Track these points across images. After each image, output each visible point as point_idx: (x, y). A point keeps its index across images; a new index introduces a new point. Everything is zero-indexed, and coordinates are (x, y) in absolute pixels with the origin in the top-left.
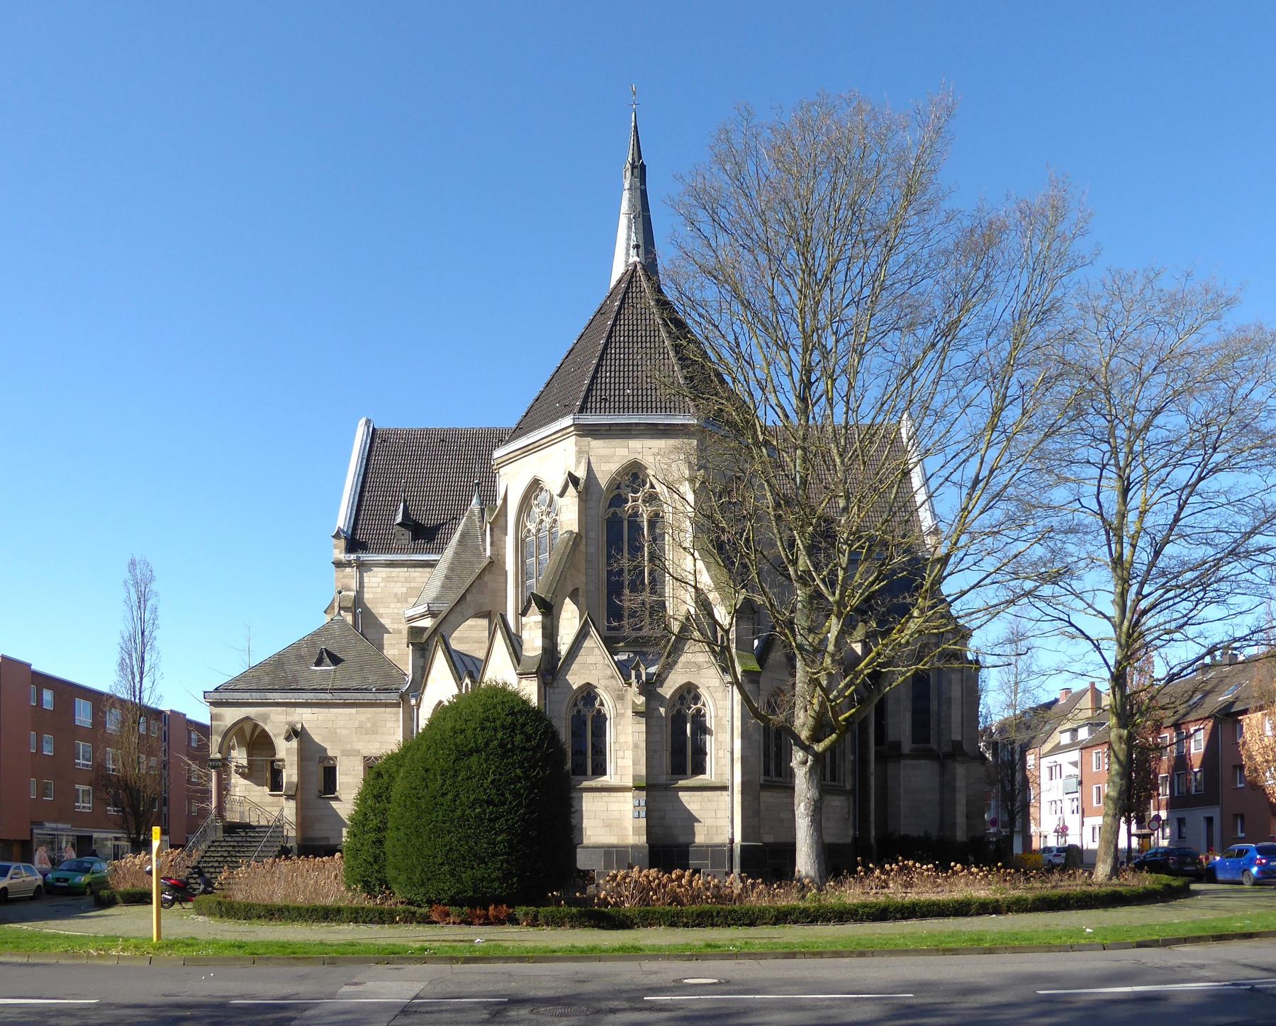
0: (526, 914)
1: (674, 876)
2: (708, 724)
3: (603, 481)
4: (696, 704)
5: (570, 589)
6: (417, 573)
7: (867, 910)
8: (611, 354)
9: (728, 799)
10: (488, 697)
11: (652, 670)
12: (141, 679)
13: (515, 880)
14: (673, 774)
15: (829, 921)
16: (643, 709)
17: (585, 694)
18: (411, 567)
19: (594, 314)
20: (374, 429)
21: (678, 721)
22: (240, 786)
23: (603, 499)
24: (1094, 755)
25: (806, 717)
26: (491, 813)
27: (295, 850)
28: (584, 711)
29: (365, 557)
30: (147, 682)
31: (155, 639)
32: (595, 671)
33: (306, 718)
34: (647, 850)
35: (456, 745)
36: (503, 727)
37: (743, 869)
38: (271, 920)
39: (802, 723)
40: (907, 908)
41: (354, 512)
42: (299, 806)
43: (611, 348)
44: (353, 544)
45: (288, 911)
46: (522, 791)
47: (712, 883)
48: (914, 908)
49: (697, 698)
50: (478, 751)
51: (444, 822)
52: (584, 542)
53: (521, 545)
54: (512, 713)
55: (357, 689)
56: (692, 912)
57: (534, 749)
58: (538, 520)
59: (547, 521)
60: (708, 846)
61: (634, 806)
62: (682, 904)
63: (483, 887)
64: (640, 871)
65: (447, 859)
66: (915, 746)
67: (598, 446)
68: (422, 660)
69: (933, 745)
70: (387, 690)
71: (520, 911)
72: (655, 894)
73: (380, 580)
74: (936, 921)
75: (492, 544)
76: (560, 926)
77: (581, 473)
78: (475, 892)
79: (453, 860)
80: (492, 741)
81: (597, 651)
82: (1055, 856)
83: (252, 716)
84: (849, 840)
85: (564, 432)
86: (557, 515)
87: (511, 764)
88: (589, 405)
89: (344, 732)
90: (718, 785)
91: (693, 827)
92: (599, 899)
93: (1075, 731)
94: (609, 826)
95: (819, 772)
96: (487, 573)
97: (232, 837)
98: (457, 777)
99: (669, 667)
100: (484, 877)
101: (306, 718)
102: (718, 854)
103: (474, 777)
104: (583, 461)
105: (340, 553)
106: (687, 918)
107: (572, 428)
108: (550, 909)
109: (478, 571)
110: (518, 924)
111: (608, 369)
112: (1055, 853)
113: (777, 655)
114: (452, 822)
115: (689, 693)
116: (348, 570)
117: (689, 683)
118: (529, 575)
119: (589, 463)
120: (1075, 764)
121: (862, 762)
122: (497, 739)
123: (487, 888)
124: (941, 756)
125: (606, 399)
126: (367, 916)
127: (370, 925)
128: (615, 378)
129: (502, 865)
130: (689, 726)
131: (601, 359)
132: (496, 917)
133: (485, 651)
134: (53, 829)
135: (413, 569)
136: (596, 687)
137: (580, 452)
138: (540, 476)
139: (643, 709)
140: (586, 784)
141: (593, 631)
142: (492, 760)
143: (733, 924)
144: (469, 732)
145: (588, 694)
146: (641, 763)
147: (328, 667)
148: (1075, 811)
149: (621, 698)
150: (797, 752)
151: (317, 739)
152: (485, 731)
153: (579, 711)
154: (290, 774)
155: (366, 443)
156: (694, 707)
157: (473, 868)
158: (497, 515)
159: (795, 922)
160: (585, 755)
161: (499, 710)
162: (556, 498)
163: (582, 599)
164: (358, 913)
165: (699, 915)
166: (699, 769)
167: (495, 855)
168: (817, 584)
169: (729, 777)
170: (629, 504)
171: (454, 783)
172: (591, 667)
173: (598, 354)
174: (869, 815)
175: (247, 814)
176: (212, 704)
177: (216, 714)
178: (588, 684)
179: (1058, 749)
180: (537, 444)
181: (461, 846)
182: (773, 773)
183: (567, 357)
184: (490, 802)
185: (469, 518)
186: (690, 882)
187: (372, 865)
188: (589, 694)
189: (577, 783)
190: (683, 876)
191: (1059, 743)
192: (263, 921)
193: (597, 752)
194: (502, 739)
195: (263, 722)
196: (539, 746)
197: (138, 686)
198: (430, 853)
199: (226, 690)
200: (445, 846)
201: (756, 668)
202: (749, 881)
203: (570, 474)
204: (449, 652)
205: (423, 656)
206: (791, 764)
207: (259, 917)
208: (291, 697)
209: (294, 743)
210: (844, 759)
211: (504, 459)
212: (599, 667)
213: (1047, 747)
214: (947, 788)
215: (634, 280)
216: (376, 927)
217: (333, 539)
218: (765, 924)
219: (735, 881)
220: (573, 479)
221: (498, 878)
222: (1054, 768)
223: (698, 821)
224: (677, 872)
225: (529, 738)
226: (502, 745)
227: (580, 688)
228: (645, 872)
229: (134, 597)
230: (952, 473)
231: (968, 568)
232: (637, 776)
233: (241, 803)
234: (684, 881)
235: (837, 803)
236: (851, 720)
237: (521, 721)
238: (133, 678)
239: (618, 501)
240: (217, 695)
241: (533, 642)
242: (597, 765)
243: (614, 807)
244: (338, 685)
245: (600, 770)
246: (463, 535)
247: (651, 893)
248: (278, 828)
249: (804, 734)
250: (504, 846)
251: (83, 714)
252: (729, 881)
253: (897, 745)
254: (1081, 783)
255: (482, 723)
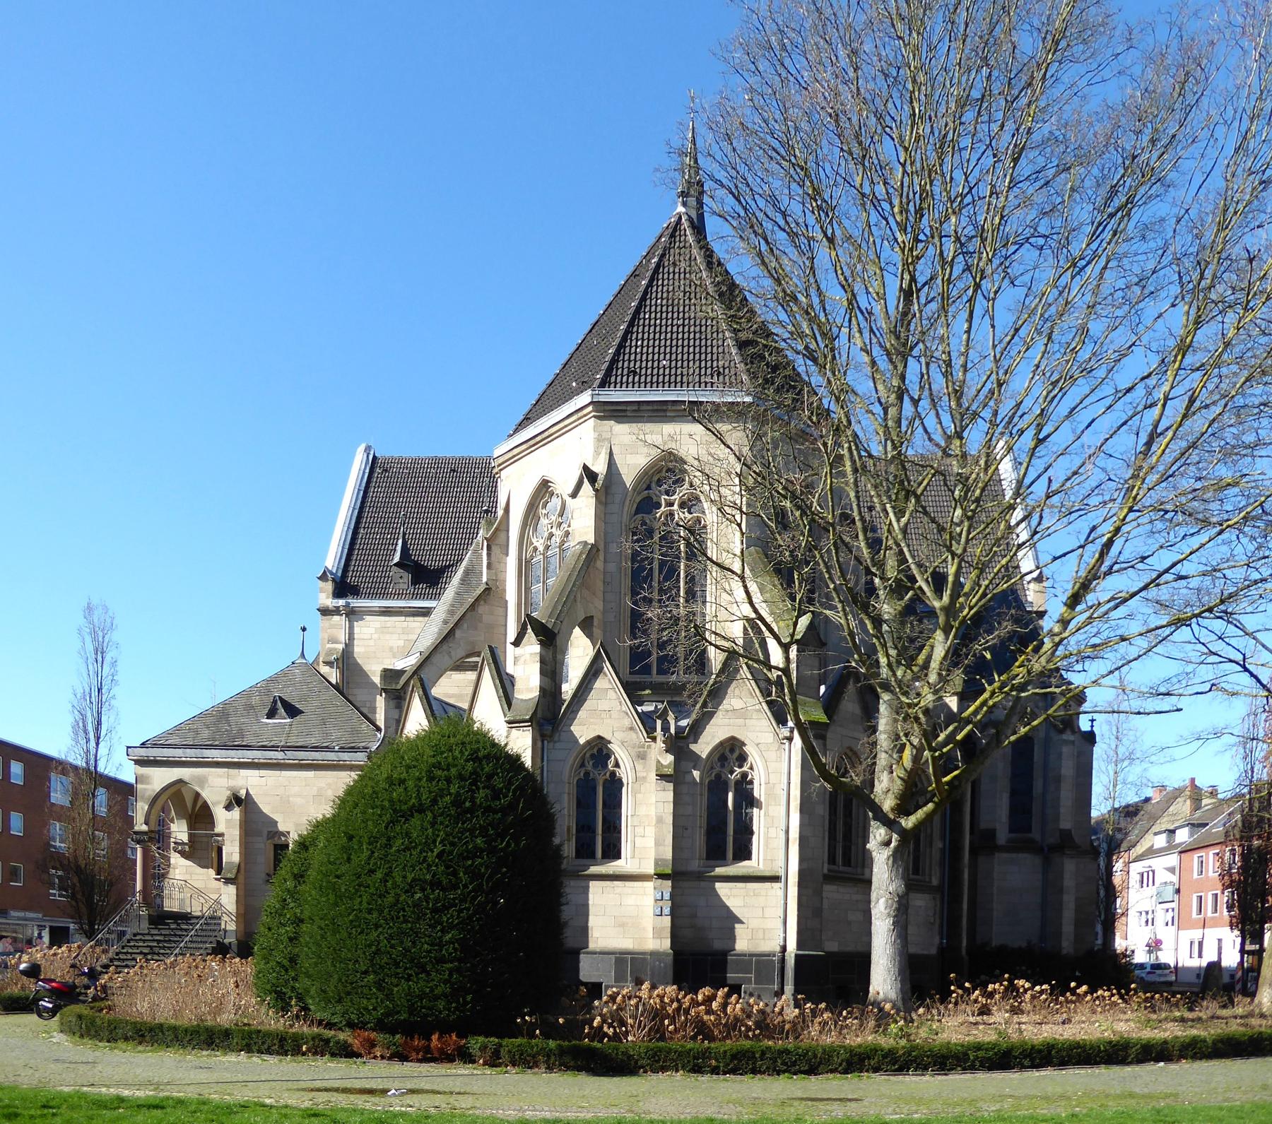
0: (483, 1048)
1: (700, 997)
2: (756, 794)
3: (629, 476)
4: (741, 767)
5: (581, 616)
6: (416, 623)
7: (981, 1054)
8: (645, 319)
9: (781, 893)
10: (443, 736)
11: (684, 723)
12: (97, 744)
13: (469, 998)
14: (708, 858)
15: (925, 1068)
16: (670, 771)
17: (595, 750)
18: (409, 616)
19: (626, 278)
20: (375, 458)
21: (717, 787)
22: (181, 868)
23: (627, 503)
24: (1196, 860)
25: (892, 780)
26: (437, 900)
27: (235, 948)
28: (594, 773)
29: (356, 603)
30: (103, 750)
31: (114, 697)
32: (609, 721)
33: (250, 782)
34: (671, 958)
35: (391, 801)
36: (461, 777)
37: (797, 991)
38: (140, 1043)
39: (886, 790)
40: (1040, 1051)
41: (346, 551)
42: (242, 893)
43: (645, 313)
44: (343, 588)
45: (162, 1032)
46: (483, 870)
47: (756, 1007)
48: (1049, 1052)
49: (742, 758)
50: (421, 810)
51: (370, 912)
52: (601, 557)
53: (525, 567)
54: (474, 757)
55: (316, 747)
56: (725, 1052)
57: (504, 811)
58: (546, 535)
59: (558, 533)
60: (752, 955)
61: (656, 900)
62: (712, 1039)
63: (422, 1007)
64: (653, 987)
65: (373, 965)
66: (1013, 835)
67: (622, 432)
68: (397, 711)
69: (1036, 835)
70: (354, 749)
71: (475, 1043)
72: (673, 1022)
73: (373, 631)
74: (1083, 1071)
75: (489, 566)
76: (530, 1068)
77: (600, 468)
78: (411, 1013)
79: (381, 967)
80: (442, 797)
81: (611, 694)
82: (1149, 973)
83: (186, 779)
84: (933, 951)
85: (580, 414)
86: (569, 526)
87: (469, 830)
88: (613, 379)
89: (299, 800)
90: (767, 874)
91: (733, 929)
92: (591, 1027)
93: (1172, 832)
94: (622, 925)
95: (905, 857)
96: (482, 602)
97: (159, 929)
98: (391, 847)
99: (706, 717)
100: (424, 993)
101: (250, 782)
102: (765, 965)
103: (415, 848)
104: (604, 450)
105: (328, 598)
106: (717, 1060)
107: (590, 408)
108: (519, 1041)
109: (471, 600)
110: (473, 1062)
111: (640, 336)
112: (1148, 969)
113: (850, 705)
114: (381, 912)
115: (732, 751)
116: (336, 618)
117: (733, 739)
118: (534, 606)
119: (611, 454)
120: (1172, 870)
121: (954, 850)
122: (450, 794)
123: (429, 1008)
124: (1046, 849)
125: (635, 373)
126: (263, 1043)
127: (265, 1057)
128: (648, 347)
129: (451, 975)
130: (730, 796)
131: (631, 324)
132: (441, 1051)
133: (469, 698)
134: (19, 918)
135: (411, 619)
136: (610, 742)
137: (599, 440)
138: (550, 476)
139: (670, 771)
140: (594, 869)
141: (607, 667)
142: (442, 823)
143: (784, 1072)
144: (410, 784)
145: (599, 750)
146: (666, 843)
147: (283, 720)
148: (1170, 923)
149: (642, 756)
150: (878, 828)
151: (266, 809)
152: (434, 783)
153: (587, 774)
154: (232, 853)
155: (364, 472)
156: (738, 770)
157: (408, 980)
158: (497, 529)
159: (876, 1070)
160: (594, 832)
161: (457, 753)
162: (569, 500)
163: (597, 632)
164: (251, 1038)
165: (734, 1057)
166: (744, 853)
167: (441, 960)
168: (920, 588)
169: (782, 864)
170: (662, 509)
171: (386, 856)
172: (603, 715)
173: (628, 318)
174: (960, 917)
175: (188, 902)
176: (138, 762)
177: (142, 775)
178: (599, 737)
179: (1151, 852)
180: (546, 434)
181: (392, 947)
182: (839, 859)
183: (590, 331)
184: (435, 884)
185: (475, 551)
186: (724, 1005)
187: (286, 970)
188: (600, 750)
189: (581, 868)
190: (714, 997)
191: (1152, 846)
192: (130, 1046)
193: (609, 828)
194: (458, 794)
195: (199, 786)
196: (512, 806)
197: (93, 751)
198: (349, 956)
199: (155, 746)
200: (370, 946)
201: (823, 718)
202: (808, 1005)
203: (585, 468)
204: (428, 701)
205: (399, 707)
206: (868, 846)
207: (126, 1039)
208: (235, 756)
209: (236, 813)
210: (931, 846)
211: (507, 457)
212: (615, 714)
213: (1139, 849)
214: (1051, 889)
215: (678, 233)
216: (272, 1060)
217: (320, 582)
218: (832, 1071)
219: (788, 1005)
220: (589, 474)
221: (445, 995)
222: (1145, 875)
223: (741, 922)
224: (707, 991)
225: (496, 795)
226: (457, 803)
227: (588, 742)
228: (659, 991)
229: (90, 647)
230: (1107, 439)
231: (1133, 567)
232: (661, 860)
233: (181, 889)
234: (715, 1005)
235: (920, 901)
236: (956, 783)
237: (487, 769)
238: (88, 741)
239: (647, 505)
240: (143, 752)
241: (528, 683)
242: (609, 846)
243: (630, 901)
244: (293, 741)
245: (613, 851)
246: (467, 572)
247: (666, 1022)
248: (215, 919)
249: (888, 804)
250: (454, 948)
251: (59, 795)
252: (779, 1004)
253: (991, 834)
254: (1178, 891)
255: (430, 771)
